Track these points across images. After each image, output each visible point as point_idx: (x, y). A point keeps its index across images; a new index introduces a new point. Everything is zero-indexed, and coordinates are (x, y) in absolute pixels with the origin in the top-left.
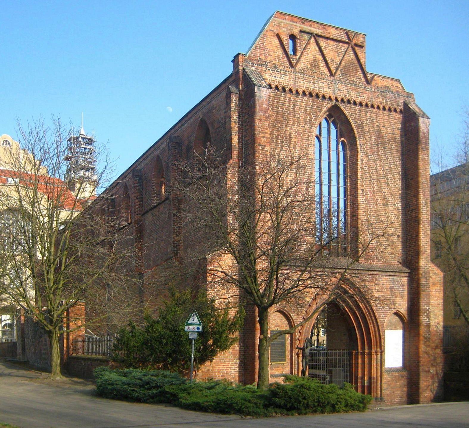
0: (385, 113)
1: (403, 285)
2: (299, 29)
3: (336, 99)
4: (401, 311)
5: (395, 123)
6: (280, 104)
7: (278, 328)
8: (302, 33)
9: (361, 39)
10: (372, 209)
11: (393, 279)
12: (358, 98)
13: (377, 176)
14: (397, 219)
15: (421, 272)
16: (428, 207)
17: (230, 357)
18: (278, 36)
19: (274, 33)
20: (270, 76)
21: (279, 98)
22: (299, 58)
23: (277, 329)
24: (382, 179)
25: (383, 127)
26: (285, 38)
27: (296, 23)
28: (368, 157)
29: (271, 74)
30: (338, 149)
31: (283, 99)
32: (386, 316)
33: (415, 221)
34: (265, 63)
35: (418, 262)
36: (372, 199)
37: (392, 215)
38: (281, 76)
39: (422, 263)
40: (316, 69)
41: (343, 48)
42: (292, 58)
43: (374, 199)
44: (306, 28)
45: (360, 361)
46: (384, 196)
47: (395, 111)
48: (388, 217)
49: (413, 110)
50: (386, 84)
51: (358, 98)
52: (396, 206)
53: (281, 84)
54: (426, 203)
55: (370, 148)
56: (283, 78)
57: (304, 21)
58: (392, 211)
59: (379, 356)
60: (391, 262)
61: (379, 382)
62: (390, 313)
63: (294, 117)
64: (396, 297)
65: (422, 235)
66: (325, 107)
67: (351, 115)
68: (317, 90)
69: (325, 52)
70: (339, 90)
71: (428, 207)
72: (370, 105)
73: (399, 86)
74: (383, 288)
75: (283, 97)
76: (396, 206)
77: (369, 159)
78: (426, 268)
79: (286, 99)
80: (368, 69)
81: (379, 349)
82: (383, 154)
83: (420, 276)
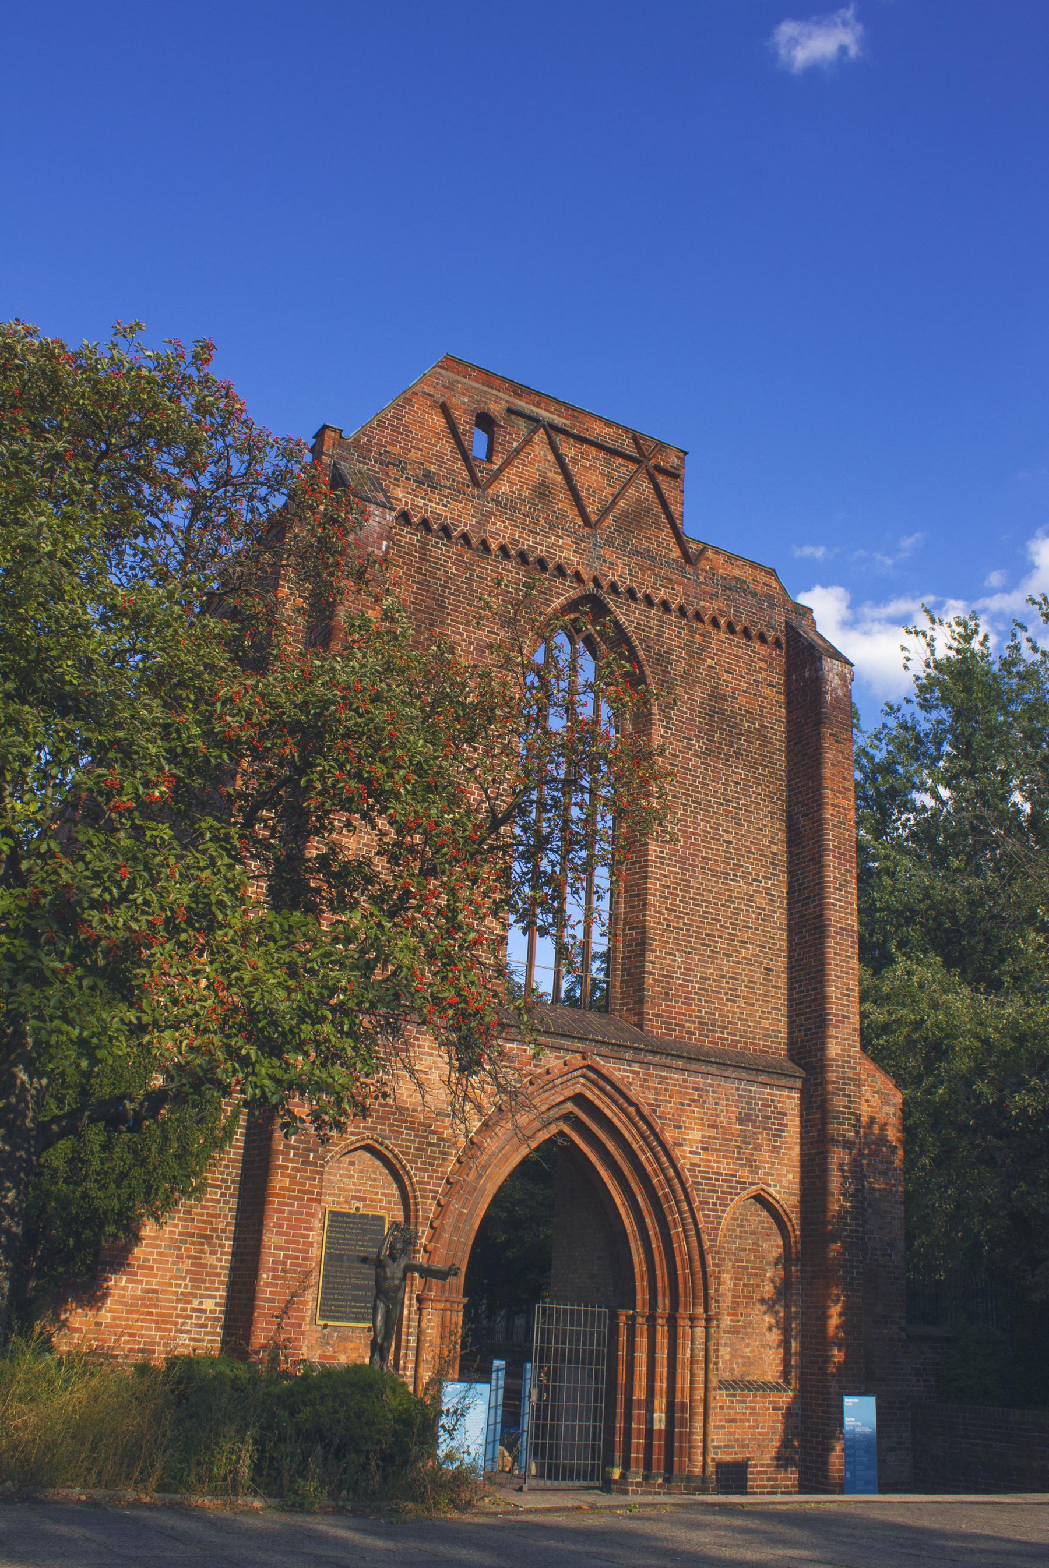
0: (733, 641)
1: (779, 1113)
2: (504, 405)
3: (595, 580)
4: (774, 1194)
5: (760, 668)
6: (430, 566)
7: (360, 1205)
8: (513, 417)
9: (674, 460)
10: (688, 881)
11: (750, 1091)
12: (658, 589)
13: (706, 795)
14: (763, 920)
15: (832, 1076)
16: (851, 893)
17: (179, 1286)
18: (445, 410)
19: (435, 401)
20: (410, 494)
21: (430, 551)
22: (500, 470)
23: (357, 1209)
24: (722, 804)
25: (726, 672)
26: (464, 421)
27: (499, 391)
28: (682, 742)
29: (414, 490)
30: (598, 710)
31: (442, 554)
32: (727, 1206)
33: (815, 929)
34: (399, 464)
35: (823, 1049)
36: (690, 854)
37: (752, 907)
38: (442, 500)
39: (833, 1049)
40: (544, 504)
41: (623, 470)
42: (479, 467)
43: (697, 856)
44: (521, 404)
45: (642, 1341)
46: (725, 851)
47: (762, 638)
48: (736, 912)
49: (807, 640)
50: (737, 572)
51: (658, 589)
52: (763, 884)
53: (438, 519)
54: (845, 880)
55: (687, 719)
56: (444, 505)
57: (519, 389)
58: (750, 898)
59: (700, 1332)
60: (746, 1043)
61: (698, 1425)
62: (737, 1194)
63: (468, 604)
64: (758, 1147)
65: (833, 970)
66: (563, 595)
67: (636, 628)
68: (542, 551)
69: (574, 470)
70: (605, 561)
71: (851, 893)
72: (690, 611)
73: (774, 584)
74: (717, 1115)
75: (439, 549)
76: (763, 884)
77: (683, 747)
78: (848, 1068)
79: (450, 557)
80: (689, 530)
81: (700, 1310)
82: (725, 740)
83: (830, 1087)
